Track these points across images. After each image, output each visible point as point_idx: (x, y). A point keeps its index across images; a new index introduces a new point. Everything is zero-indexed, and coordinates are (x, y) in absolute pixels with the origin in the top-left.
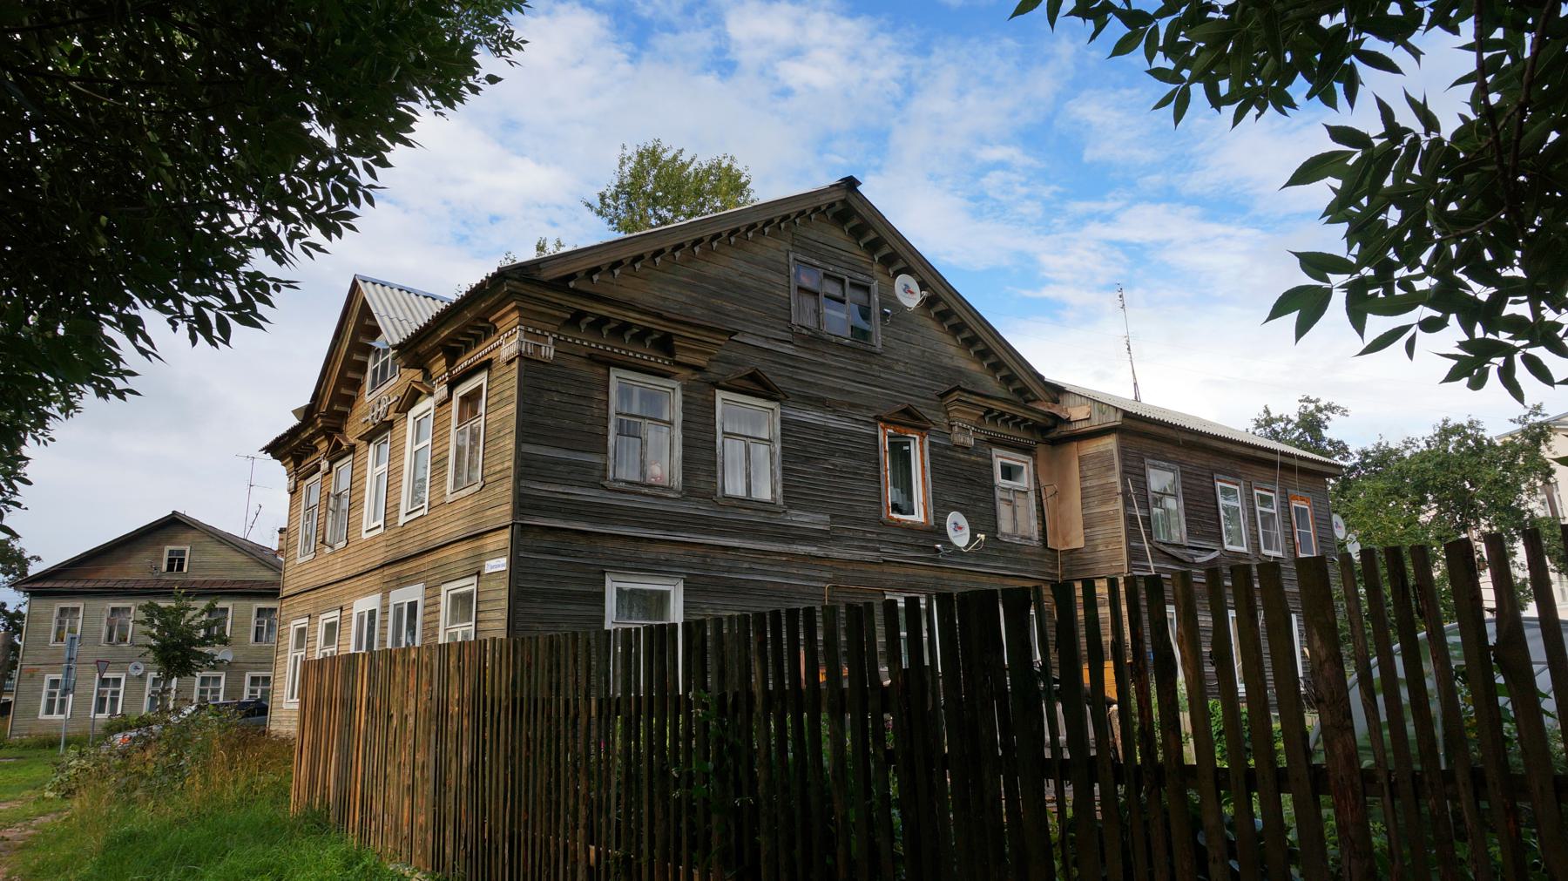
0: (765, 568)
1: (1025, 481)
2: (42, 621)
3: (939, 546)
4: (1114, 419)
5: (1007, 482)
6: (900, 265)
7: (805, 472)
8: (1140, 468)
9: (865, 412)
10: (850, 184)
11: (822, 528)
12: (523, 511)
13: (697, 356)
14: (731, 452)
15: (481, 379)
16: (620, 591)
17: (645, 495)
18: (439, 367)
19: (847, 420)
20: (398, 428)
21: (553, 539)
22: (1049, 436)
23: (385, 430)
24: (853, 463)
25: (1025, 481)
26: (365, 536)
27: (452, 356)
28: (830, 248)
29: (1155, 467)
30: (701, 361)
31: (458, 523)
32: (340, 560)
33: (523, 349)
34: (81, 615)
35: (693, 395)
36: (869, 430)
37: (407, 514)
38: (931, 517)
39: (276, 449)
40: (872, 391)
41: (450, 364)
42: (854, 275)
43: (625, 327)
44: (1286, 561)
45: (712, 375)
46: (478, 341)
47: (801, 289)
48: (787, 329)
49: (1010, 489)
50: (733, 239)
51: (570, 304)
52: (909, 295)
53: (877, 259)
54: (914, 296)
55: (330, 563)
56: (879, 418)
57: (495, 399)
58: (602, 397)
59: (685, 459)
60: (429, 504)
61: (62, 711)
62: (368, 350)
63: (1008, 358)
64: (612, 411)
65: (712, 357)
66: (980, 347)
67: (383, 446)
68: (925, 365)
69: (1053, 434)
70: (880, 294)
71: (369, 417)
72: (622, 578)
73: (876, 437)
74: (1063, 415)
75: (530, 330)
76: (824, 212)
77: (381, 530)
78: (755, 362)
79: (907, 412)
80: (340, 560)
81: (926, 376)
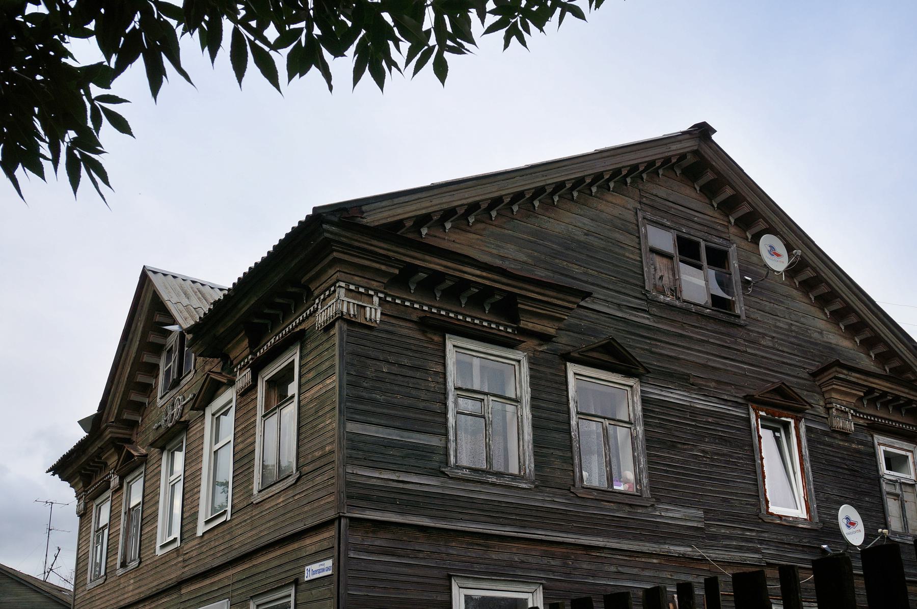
0: (635, 571)
3: (825, 546)
5: (892, 473)
6: (762, 225)
7: (672, 459)
10: (703, 131)
11: (695, 524)
12: (350, 502)
13: (545, 322)
15: (294, 356)
16: (468, 598)
18: (241, 350)
20: (194, 429)
21: (389, 536)
24: (725, 450)
26: (159, 552)
30: (549, 328)
31: (268, 525)
32: (132, 581)
33: (345, 310)
35: (542, 369)
36: (739, 412)
37: (207, 522)
38: (815, 513)
41: (254, 344)
43: (463, 285)
45: (560, 346)
46: (287, 312)
47: (653, 251)
48: (641, 296)
49: (896, 481)
50: (575, 194)
55: (121, 586)
56: (750, 399)
57: (311, 375)
58: (439, 369)
62: (158, 349)
64: (450, 386)
65: (561, 325)
66: (853, 319)
67: (177, 453)
68: (793, 340)
70: (739, 260)
72: (471, 584)
73: (748, 420)
75: (352, 287)
77: (178, 544)
78: (609, 331)
79: (781, 390)
80: (132, 581)
81: (796, 352)
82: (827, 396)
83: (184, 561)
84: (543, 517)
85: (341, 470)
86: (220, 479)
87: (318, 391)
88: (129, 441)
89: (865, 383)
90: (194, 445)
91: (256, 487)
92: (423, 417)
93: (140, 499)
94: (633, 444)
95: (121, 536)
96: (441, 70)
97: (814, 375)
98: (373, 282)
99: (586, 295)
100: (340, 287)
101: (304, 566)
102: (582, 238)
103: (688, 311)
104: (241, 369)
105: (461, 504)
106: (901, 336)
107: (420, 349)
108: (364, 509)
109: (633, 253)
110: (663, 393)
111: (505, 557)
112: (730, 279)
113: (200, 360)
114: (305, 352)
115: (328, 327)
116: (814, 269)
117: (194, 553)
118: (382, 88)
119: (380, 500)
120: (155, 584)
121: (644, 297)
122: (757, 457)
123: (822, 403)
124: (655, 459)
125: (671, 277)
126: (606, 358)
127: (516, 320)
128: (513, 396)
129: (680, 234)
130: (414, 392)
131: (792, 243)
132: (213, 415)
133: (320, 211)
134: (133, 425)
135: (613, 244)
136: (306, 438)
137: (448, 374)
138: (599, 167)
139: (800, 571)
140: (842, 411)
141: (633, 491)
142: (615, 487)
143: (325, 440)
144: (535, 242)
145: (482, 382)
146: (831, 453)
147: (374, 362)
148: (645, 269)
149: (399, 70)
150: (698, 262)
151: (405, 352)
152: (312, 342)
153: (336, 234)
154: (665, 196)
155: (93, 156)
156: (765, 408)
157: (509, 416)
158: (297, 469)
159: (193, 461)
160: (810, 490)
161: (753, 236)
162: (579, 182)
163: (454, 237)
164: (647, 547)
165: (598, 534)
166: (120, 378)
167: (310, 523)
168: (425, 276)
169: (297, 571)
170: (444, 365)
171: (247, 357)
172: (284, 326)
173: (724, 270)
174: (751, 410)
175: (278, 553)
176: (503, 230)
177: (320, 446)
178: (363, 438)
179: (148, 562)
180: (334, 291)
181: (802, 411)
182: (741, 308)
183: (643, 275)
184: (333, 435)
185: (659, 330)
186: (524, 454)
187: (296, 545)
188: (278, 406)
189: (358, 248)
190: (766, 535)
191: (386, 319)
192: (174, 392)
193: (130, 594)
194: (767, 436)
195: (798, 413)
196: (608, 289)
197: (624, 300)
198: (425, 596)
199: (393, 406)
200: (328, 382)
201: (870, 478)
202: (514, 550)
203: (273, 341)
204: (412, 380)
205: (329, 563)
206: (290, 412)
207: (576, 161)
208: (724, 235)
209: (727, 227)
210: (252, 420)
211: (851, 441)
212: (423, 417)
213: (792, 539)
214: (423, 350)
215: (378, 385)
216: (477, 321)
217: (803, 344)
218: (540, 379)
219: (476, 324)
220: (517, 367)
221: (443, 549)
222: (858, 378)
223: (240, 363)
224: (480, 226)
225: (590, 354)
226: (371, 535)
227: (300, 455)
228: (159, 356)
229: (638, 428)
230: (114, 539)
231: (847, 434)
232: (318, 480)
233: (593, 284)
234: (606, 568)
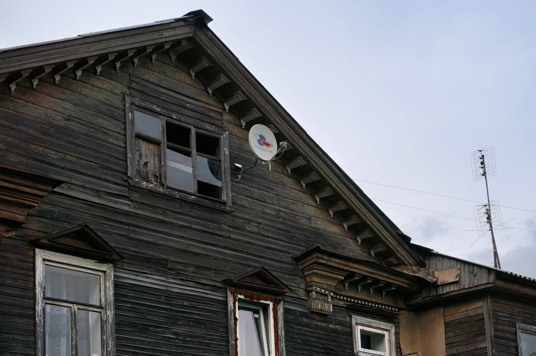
4: (483, 280)
6: (255, 114)
7: (142, 342)
8: (511, 333)
9: (212, 275)
13: (13, 209)
19: (191, 284)
24: (199, 332)
29: (526, 331)
30: (19, 216)
36: (217, 296)
40: (221, 253)
42: (201, 124)
45: (30, 233)
50: (58, 78)
53: (227, 108)
54: (270, 149)
56: (228, 283)
63: (372, 218)
65: (32, 211)
66: (341, 207)
68: (279, 226)
69: (419, 300)
70: (230, 148)
73: (226, 303)
74: (430, 278)
76: (167, 52)
81: (281, 237)
82: (308, 279)
89: (346, 268)
94: (102, 327)
99: (59, 183)
102: (62, 123)
106: (385, 223)
109: (117, 139)
116: (305, 158)
121: (126, 184)
123: (303, 286)
125: (157, 163)
135: (96, 129)
140: (322, 294)
146: (308, 333)
148: (129, 155)
154: (156, 81)
173: (214, 157)
174: (229, 294)
181: (282, 294)
183: (126, 161)
185: (139, 216)
197: (104, 186)
208: (216, 122)
217: (289, 229)
222: (338, 263)
229: (109, 313)
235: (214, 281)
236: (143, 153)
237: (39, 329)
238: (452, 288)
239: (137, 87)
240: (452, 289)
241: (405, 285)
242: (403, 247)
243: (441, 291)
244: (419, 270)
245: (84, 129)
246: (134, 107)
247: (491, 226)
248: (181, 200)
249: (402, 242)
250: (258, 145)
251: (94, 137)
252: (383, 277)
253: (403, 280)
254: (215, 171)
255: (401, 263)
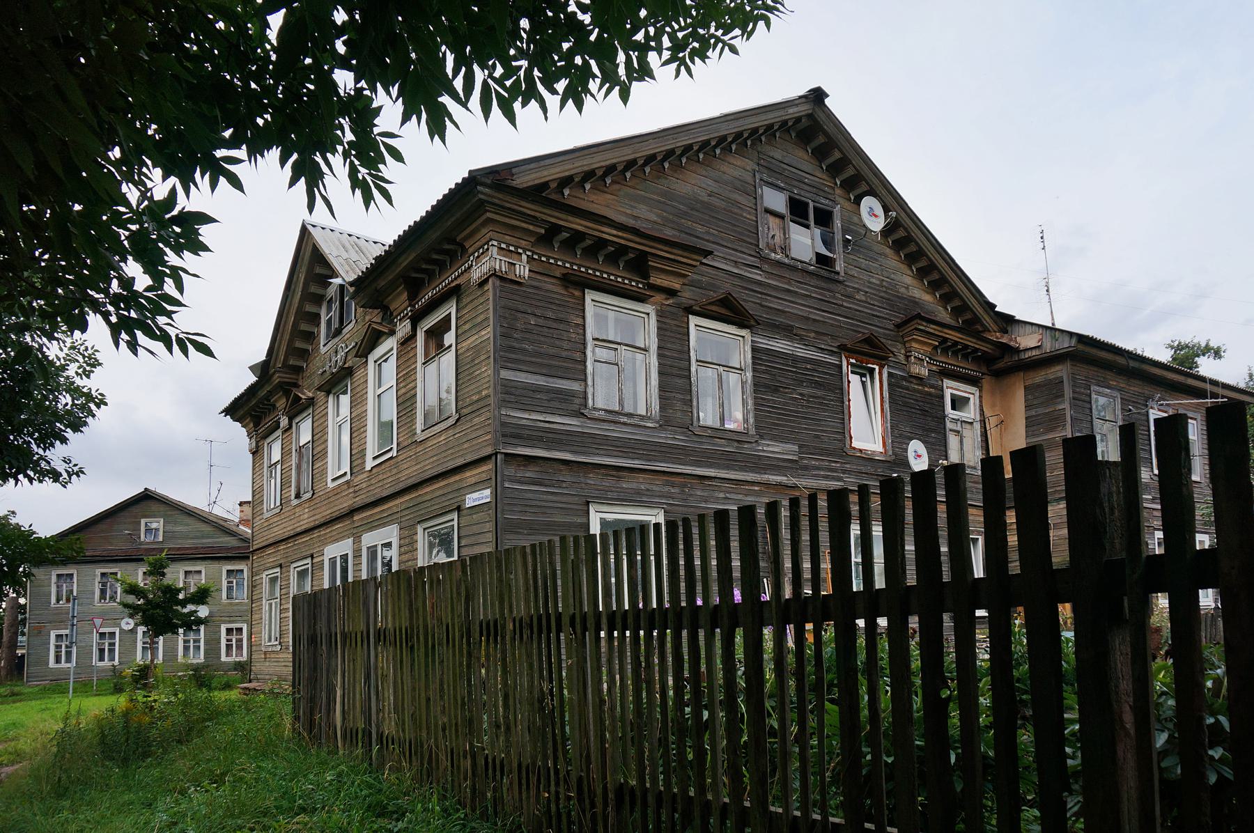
1: (971, 413)
2: (43, 586)
4: (1065, 344)
5: (955, 412)
6: (864, 187)
7: (775, 402)
9: (828, 339)
10: (817, 96)
11: (790, 457)
13: (671, 278)
14: (704, 378)
15: (451, 309)
17: (625, 424)
18: (400, 302)
20: (358, 374)
22: (996, 367)
23: (343, 378)
24: (819, 393)
25: (971, 413)
26: (331, 485)
27: (414, 290)
28: (794, 170)
30: (675, 284)
31: (431, 460)
32: (307, 510)
33: (498, 267)
34: (75, 580)
36: (833, 360)
37: (375, 458)
38: (889, 447)
39: (235, 410)
41: (413, 297)
43: (601, 243)
44: (1202, 485)
45: (684, 300)
46: (442, 267)
47: (768, 211)
50: (701, 156)
51: (544, 217)
52: (873, 216)
53: (838, 183)
54: (879, 220)
56: (843, 348)
57: (467, 327)
58: (579, 321)
59: (662, 388)
60: (398, 444)
61: (68, 660)
62: (318, 299)
65: (686, 281)
66: (935, 276)
68: (882, 294)
69: (1001, 365)
71: (327, 368)
72: (605, 508)
73: (840, 367)
74: (1012, 344)
75: (503, 246)
77: (348, 477)
78: (726, 286)
79: (870, 341)
80: (307, 510)
81: (885, 306)
82: (907, 345)
83: (355, 492)
84: (667, 452)
85: (496, 412)
86: (385, 418)
87: (474, 342)
88: (296, 385)
89: (940, 334)
90: (358, 390)
91: (419, 425)
92: (566, 364)
93: (310, 438)
94: (743, 387)
95: (293, 471)
96: (625, 96)
97: (898, 326)
98: (521, 241)
99: (707, 253)
100: (492, 245)
101: (465, 495)
102: (706, 199)
103: (795, 268)
104: (400, 320)
105: (598, 441)
106: (974, 291)
107: (562, 303)
108: (517, 445)
109: (749, 213)
110: (770, 343)
111: (634, 486)
112: (833, 238)
113: (360, 310)
114: (461, 305)
115: (483, 283)
116: (906, 229)
117: (364, 485)
118: (580, 112)
119: (529, 438)
120: (328, 512)
121: (758, 255)
122: (846, 399)
123: (903, 351)
124: (761, 402)
125: (782, 235)
126: (723, 311)
127: (646, 276)
128: (643, 346)
129: (792, 195)
130: (557, 342)
131: (888, 204)
132: (375, 362)
133: (474, 174)
134: (298, 370)
135: (733, 204)
136: (463, 383)
137: (587, 326)
138: (724, 130)
139: (872, 495)
140: (919, 358)
141: (741, 429)
142: (726, 426)
143: (481, 385)
144: (664, 203)
145: (616, 333)
146: (907, 396)
147: (523, 315)
148: (760, 228)
149: (593, 95)
150: (806, 222)
151: (550, 306)
152: (467, 296)
153: (489, 196)
154: (780, 158)
155: (382, 184)
156: (855, 356)
157: (638, 363)
158: (456, 412)
159: (358, 404)
160: (887, 427)
161: (855, 197)
162: (705, 144)
163: (593, 197)
164: (750, 477)
165: (710, 466)
166: (284, 326)
167: (469, 458)
168: (568, 235)
169: (459, 499)
170: (584, 318)
171: (406, 309)
172: (441, 281)
173: (828, 229)
174: (843, 358)
175: (442, 484)
176: (636, 191)
177: (477, 390)
178: (516, 384)
179: (321, 494)
180: (488, 249)
181: (886, 358)
182: (840, 265)
183: (758, 234)
184: (489, 381)
185: (769, 285)
186: (651, 397)
187: (457, 478)
188: (438, 355)
189: (509, 209)
190: (848, 466)
191: (533, 275)
192: (336, 340)
193: (305, 522)
194: (855, 380)
195: (882, 360)
196: (729, 248)
197: (740, 258)
198: (568, 519)
199: (540, 355)
200: (483, 333)
201: (937, 417)
202: (641, 480)
203: (430, 294)
204: (556, 331)
205: (487, 492)
206: (448, 360)
207: (702, 124)
208: (830, 196)
209: (833, 189)
210: (413, 367)
211: (924, 385)
212: (566, 364)
213: (870, 469)
214: (565, 304)
215: (527, 336)
216: (612, 278)
217: (892, 298)
218: (666, 330)
219: (612, 280)
220: (646, 320)
221: (582, 480)
222: (935, 329)
223: (400, 314)
224: (616, 187)
225: (708, 307)
226: (522, 468)
227: (459, 399)
228: (320, 306)
229: (748, 374)
230: (288, 474)
231: (921, 379)
232: (476, 420)
233: (714, 243)
234: (716, 494)
235: (831, 346)
236: (771, 227)
237: (694, 388)
238: (1034, 353)
239: (764, 164)
240: (1034, 354)
241: (990, 351)
242: (988, 314)
243: (1022, 356)
244: (1002, 337)
245: (723, 204)
246: (763, 183)
247: (1050, 298)
248: (803, 271)
249: (988, 309)
250: (868, 216)
251: (731, 212)
252: (971, 342)
253: (988, 346)
254: (827, 243)
255: (987, 330)
